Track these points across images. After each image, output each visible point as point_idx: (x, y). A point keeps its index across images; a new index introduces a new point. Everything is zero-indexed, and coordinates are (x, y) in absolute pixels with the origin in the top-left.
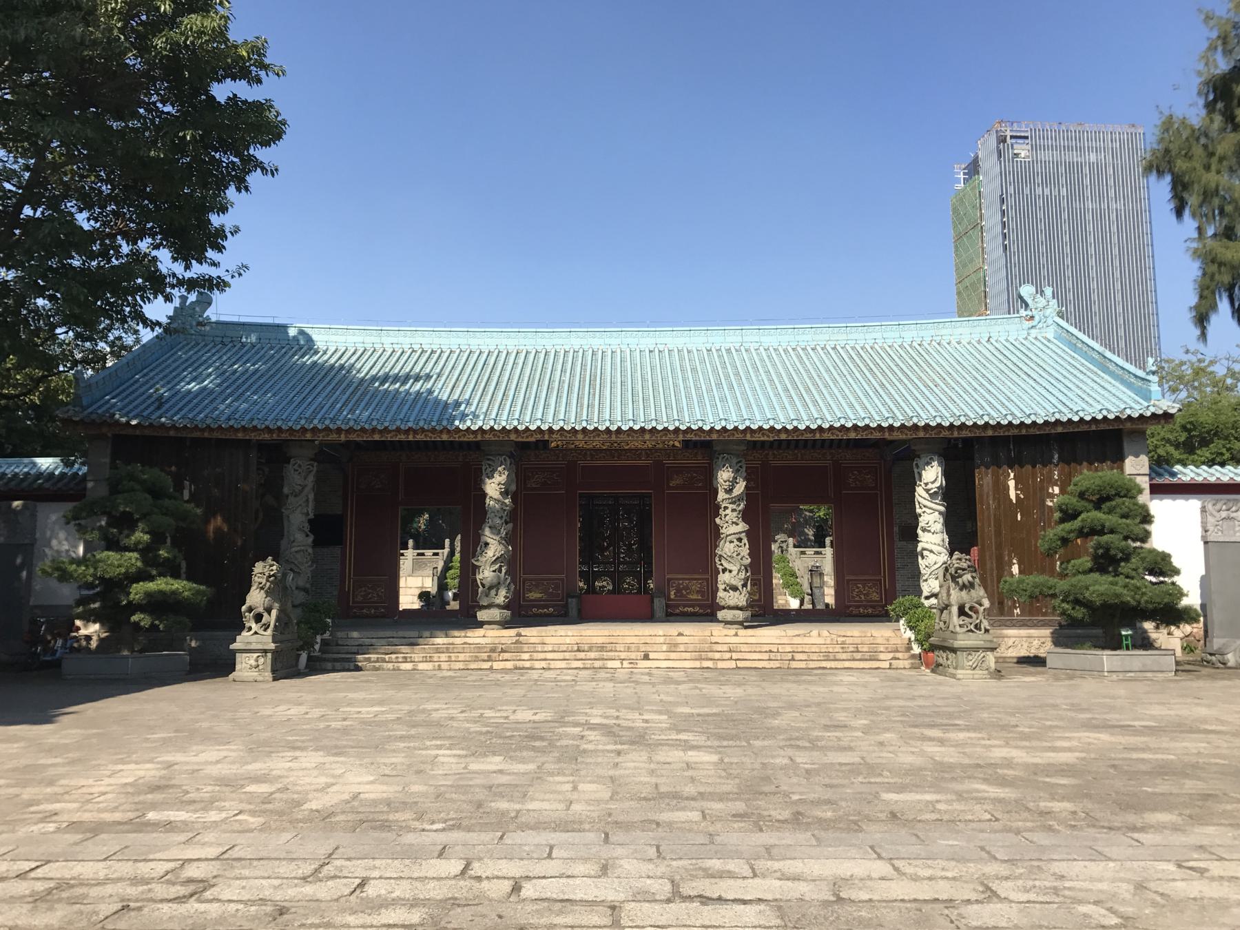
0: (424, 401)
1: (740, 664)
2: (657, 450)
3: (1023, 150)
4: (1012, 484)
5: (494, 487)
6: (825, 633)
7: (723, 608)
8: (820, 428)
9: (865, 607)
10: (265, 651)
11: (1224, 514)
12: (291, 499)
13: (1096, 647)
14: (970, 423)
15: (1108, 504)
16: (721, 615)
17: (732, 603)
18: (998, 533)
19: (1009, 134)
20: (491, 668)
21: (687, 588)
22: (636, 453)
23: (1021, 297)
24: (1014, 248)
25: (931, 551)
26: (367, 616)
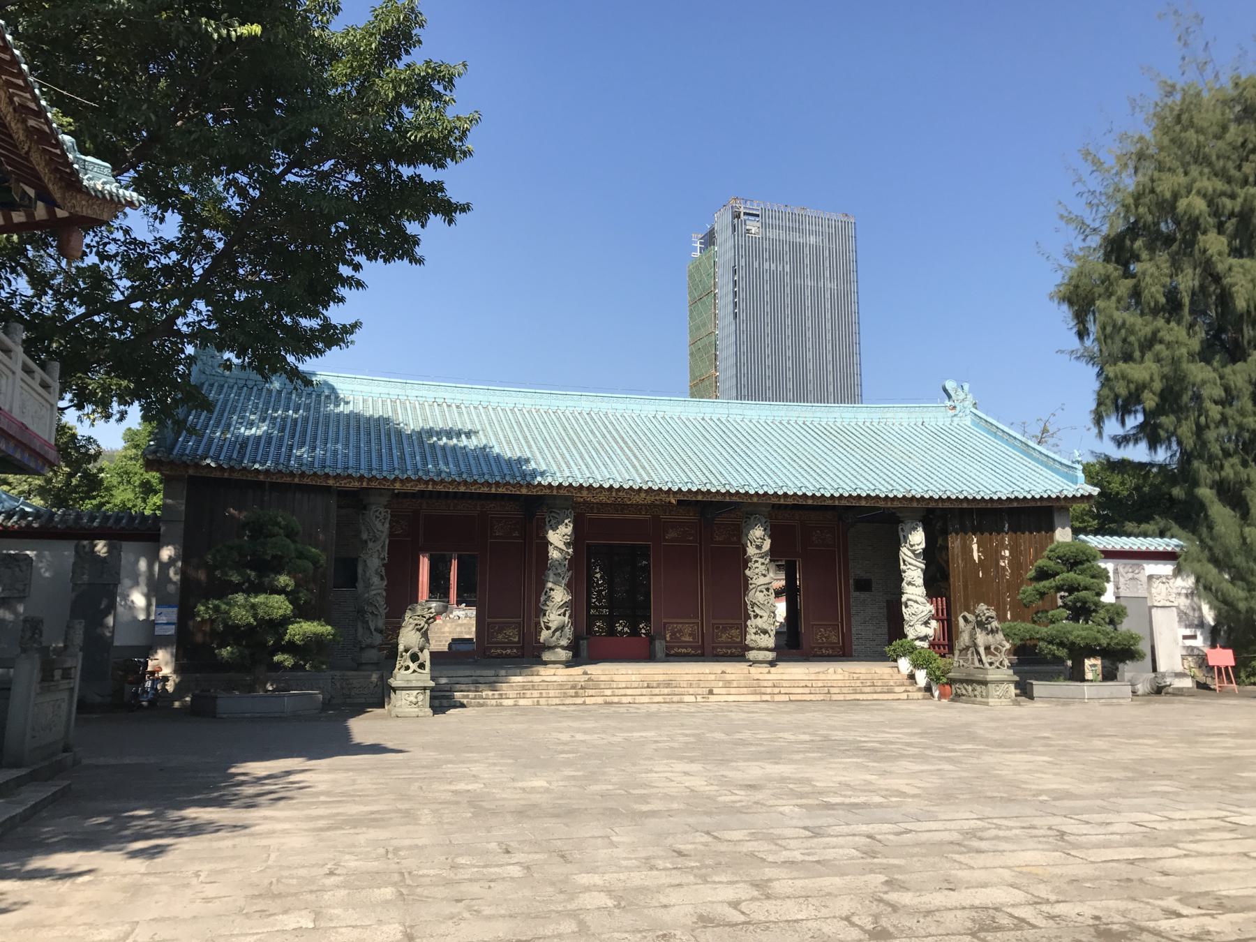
0: (483, 454)
1: (793, 697)
2: (655, 506)
3: (753, 226)
4: (975, 547)
5: (559, 538)
6: (840, 671)
7: (752, 649)
8: (785, 494)
9: (827, 648)
10: (425, 688)
11: (1130, 575)
12: (370, 545)
13: (1066, 679)
14: (882, 495)
15: (1080, 567)
16: (752, 655)
17: (763, 645)
18: (966, 587)
19: (742, 210)
20: (584, 704)
21: (680, 631)
22: (637, 507)
23: (945, 390)
24: (743, 316)
25: (916, 602)
26: (500, 656)
